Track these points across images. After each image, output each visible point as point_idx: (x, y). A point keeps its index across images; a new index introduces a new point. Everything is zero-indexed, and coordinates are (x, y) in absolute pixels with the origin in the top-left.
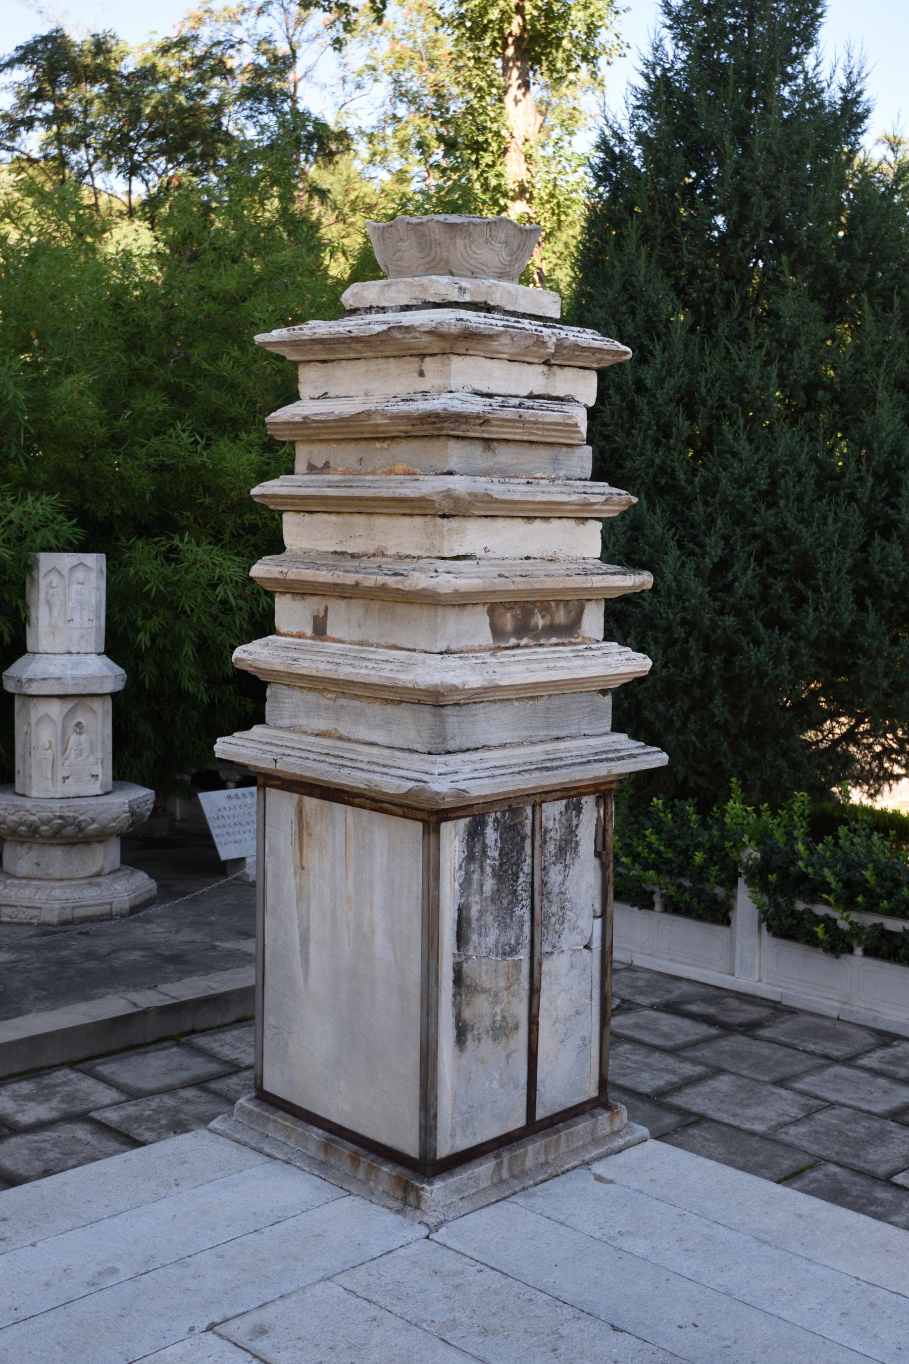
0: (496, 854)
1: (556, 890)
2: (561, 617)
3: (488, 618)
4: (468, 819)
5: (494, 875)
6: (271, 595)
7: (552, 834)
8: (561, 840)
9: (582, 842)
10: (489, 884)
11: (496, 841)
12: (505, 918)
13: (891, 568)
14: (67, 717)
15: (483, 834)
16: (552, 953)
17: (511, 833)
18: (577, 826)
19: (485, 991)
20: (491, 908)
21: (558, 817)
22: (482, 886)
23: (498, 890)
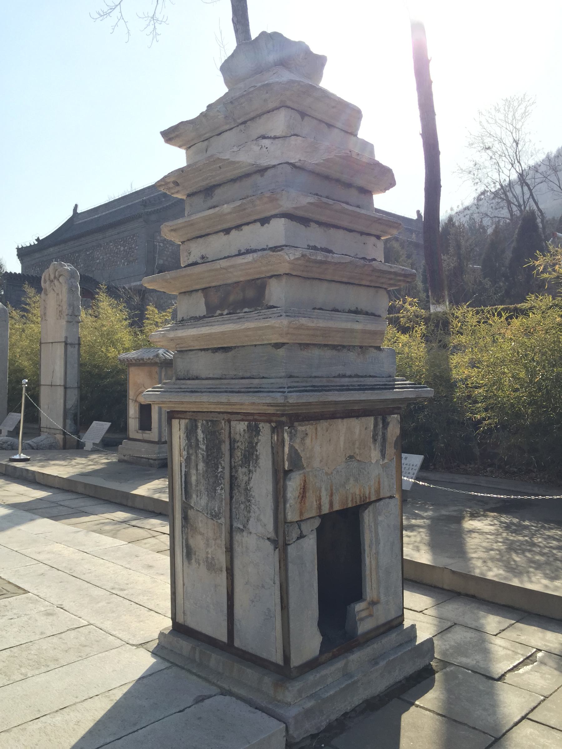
0: (204, 447)
1: (243, 485)
2: (251, 293)
3: (204, 299)
4: (187, 421)
5: (204, 461)
6: (124, 372)
7: (239, 444)
8: (245, 451)
9: (261, 457)
10: (201, 466)
11: (203, 438)
12: (212, 492)
13: (469, 234)
14: (417, 245)
15: (196, 433)
16: (242, 531)
17: (213, 436)
18: (257, 443)
19: (202, 534)
20: (202, 481)
21: (242, 433)
22: (197, 465)
23: (207, 471)
